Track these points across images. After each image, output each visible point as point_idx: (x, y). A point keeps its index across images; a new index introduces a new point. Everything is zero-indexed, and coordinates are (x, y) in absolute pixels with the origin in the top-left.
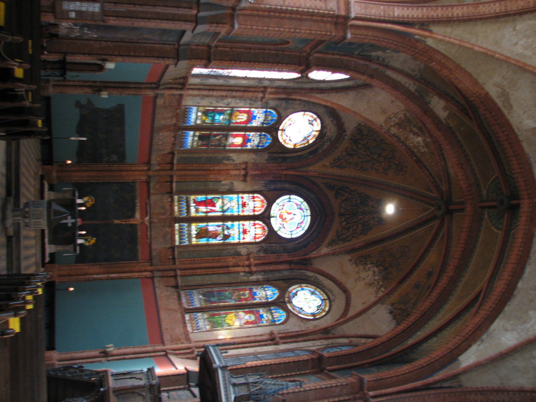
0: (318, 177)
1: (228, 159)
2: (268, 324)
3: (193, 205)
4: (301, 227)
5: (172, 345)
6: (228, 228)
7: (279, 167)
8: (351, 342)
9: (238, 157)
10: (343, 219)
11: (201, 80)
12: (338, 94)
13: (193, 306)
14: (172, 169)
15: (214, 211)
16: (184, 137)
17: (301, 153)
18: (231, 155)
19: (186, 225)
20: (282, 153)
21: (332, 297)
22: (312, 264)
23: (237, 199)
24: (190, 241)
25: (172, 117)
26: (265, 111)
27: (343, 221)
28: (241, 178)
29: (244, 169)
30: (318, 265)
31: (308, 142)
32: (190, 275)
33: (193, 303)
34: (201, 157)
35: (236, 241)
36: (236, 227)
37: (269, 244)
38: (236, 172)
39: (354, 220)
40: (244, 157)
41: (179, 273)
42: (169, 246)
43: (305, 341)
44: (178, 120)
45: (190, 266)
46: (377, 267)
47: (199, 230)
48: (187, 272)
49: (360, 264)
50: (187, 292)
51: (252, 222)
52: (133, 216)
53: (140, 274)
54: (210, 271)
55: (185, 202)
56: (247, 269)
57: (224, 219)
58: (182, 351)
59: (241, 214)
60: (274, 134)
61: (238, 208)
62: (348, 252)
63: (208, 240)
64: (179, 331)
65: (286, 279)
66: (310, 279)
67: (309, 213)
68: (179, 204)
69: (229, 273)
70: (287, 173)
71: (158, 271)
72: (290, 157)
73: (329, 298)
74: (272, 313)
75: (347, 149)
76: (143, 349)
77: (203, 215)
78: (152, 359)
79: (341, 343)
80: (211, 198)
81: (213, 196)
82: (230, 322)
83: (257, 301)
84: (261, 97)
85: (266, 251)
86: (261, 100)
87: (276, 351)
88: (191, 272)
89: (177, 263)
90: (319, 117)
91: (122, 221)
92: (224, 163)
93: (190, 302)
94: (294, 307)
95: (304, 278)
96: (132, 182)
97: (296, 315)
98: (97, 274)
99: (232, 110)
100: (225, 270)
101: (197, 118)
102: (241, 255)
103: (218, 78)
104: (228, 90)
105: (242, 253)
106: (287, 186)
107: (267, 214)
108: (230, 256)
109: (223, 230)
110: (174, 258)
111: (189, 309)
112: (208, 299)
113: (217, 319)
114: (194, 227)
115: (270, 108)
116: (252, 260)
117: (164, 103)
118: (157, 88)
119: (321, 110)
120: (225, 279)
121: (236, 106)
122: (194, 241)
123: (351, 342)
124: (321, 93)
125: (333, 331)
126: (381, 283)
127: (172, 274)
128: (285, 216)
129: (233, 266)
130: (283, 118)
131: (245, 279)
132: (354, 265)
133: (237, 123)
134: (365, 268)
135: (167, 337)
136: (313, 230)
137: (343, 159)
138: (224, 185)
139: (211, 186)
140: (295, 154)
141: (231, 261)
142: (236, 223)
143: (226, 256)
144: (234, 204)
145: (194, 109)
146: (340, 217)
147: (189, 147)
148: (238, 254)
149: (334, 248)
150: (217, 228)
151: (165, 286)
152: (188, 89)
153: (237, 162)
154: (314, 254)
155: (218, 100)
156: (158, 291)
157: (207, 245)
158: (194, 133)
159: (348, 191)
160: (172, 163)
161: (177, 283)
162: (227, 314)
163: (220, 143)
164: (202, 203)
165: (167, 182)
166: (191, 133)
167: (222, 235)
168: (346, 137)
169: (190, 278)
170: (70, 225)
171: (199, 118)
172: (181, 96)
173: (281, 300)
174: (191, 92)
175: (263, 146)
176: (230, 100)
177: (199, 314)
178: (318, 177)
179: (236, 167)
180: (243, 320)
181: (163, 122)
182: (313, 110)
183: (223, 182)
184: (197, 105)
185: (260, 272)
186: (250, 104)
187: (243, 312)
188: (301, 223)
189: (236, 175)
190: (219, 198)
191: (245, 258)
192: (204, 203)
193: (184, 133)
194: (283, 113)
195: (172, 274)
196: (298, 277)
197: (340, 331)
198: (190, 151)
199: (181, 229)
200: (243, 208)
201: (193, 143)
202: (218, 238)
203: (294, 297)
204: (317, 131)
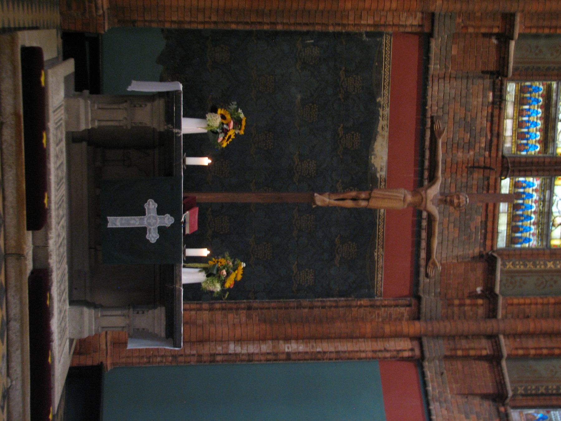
19: (536, 182)
32: (539, 357)
41: (506, 347)
42: (477, 251)
53: (379, 345)
55: (541, 107)
68: (520, 113)
71: (437, 336)
96: (368, 34)
98: (239, 341)
151: (460, 394)
161: (501, 384)
170: (153, 237)
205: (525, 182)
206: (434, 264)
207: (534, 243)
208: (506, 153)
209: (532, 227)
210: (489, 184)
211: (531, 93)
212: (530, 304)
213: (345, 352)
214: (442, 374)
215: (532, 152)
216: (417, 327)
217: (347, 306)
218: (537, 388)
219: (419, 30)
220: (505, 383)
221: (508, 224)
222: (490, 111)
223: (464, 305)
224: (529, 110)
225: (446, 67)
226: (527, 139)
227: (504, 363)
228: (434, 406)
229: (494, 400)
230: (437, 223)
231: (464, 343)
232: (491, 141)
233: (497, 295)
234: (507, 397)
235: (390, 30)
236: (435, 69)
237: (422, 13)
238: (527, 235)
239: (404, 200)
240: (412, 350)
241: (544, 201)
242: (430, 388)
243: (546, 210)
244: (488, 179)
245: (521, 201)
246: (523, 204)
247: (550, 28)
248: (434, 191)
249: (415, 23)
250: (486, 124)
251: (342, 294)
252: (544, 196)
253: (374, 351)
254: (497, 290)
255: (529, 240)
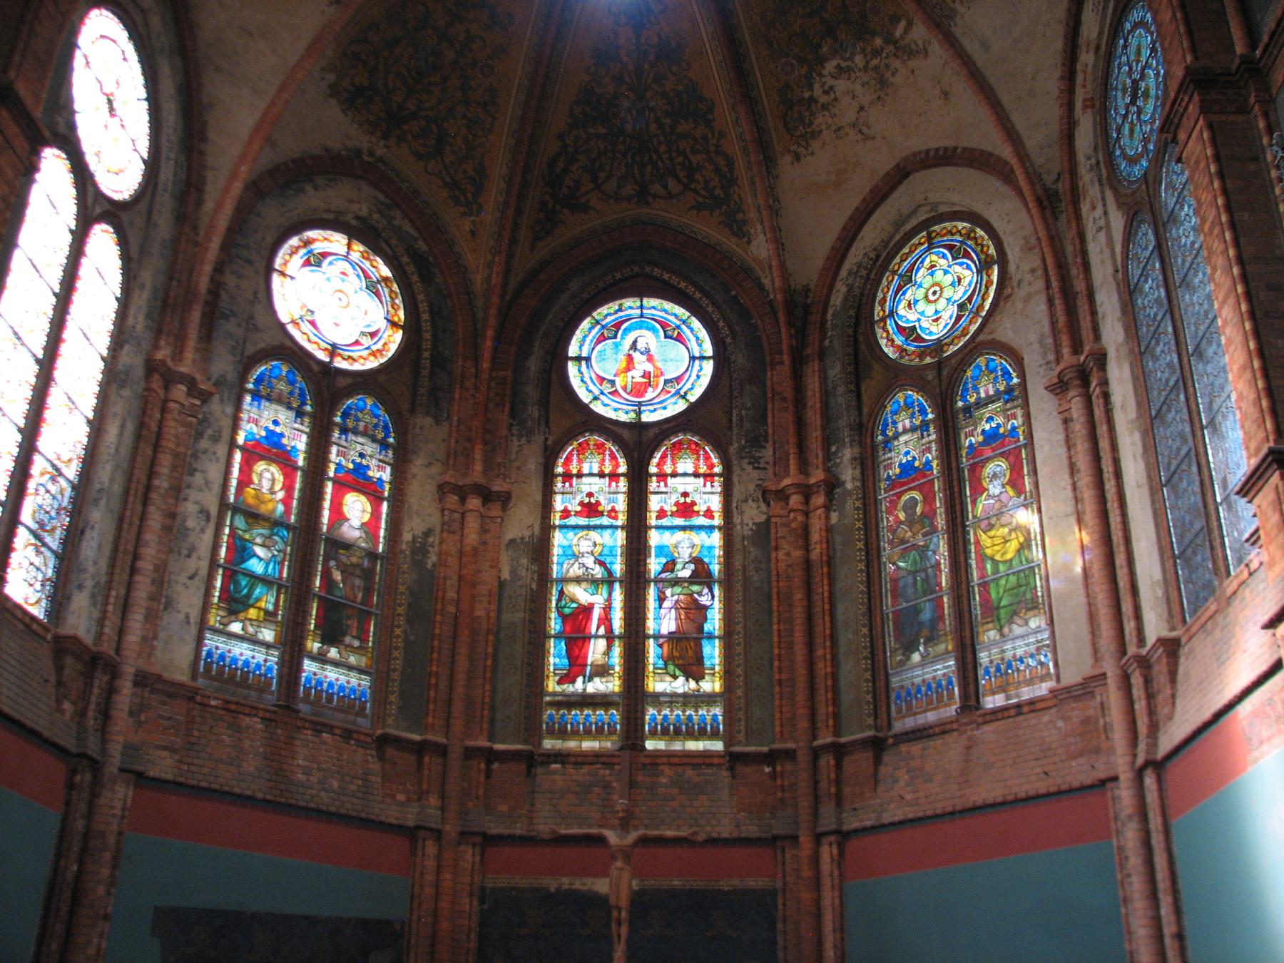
0: (510, 255)
1: (420, 549)
2: (1019, 412)
3: (579, 684)
4: (678, 327)
5: (1112, 750)
6: (670, 566)
7: (468, 384)
8: (1089, 104)
9: (418, 513)
10: (657, 188)
11: (80, 587)
12: (212, 134)
13: (950, 683)
14: (442, 751)
15: (608, 608)
16: (323, 697)
17: (423, 307)
18: (407, 537)
19: (651, 711)
20: (416, 368)
21: (922, 216)
22: (806, 290)
23: (571, 534)
24: (709, 699)
25: (236, 728)
26: (253, 400)
27: (665, 187)
28: (495, 511)
29: (463, 500)
30: (809, 268)
31: (386, 279)
32: (836, 701)
33: (939, 685)
34: (407, 641)
35: (716, 539)
36: (668, 539)
37: (730, 428)
38: (472, 523)
39: (663, 148)
40: (421, 494)
41: (825, 739)
42: (725, 773)
43: (1086, 267)
44: (253, 710)
45: (801, 696)
46: (821, 61)
47: (671, 668)
48: (823, 710)
49: (811, 123)
50: (899, 711)
51: (653, 484)
52: (599, 902)
53: (826, 882)
54: (822, 627)
55: (569, 711)
56: (819, 500)
57: (635, 581)
58: (1140, 706)
59: (622, 519)
60: (342, 382)
61: (602, 527)
62: (770, 164)
63: (711, 636)
64: (1052, 728)
65: (857, 369)
66: (857, 291)
67: (630, 303)
68: (575, 733)
69: (830, 562)
70: (487, 354)
71: (816, 814)
72: (436, 339)
73: (925, 225)
74: (980, 404)
75: (419, 156)
76: (1135, 861)
77: (617, 650)
78: (1177, 825)
79: (1095, 137)
80: (559, 621)
81: (553, 615)
82: (1013, 546)
83: (932, 456)
84: (190, 394)
85: (757, 441)
86: (205, 397)
87: (1131, 352)
88: (823, 696)
89: (790, 745)
90: (297, 228)
91: (616, 939)
92: (434, 565)
93: (936, 693)
94: (952, 335)
95: (852, 312)
96: (482, 902)
97: (986, 320)
99: (236, 509)
100: (819, 573)
101: (253, 641)
102: (768, 521)
103: (81, 525)
104: (145, 502)
105: (763, 518)
106: (533, 365)
107: (626, 434)
108: (769, 560)
109: (676, 582)
110: (771, 758)
111: (965, 696)
112: (925, 632)
113: (1001, 591)
114: (656, 685)
115: (243, 378)
116: (787, 481)
117: (171, 749)
118: (96, 766)
119: (271, 213)
120: (851, 576)
121: (216, 488)
122: (711, 685)
123: (1089, 104)
124: (200, 190)
125: (1049, 179)
126: (878, 42)
127: (827, 761)
128: (636, 375)
129: (807, 548)
130: (288, 343)
131: (851, 504)
132: (815, 145)
133: (286, 502)
134: (825, 107)
135: (1079, 772)
136: (691, 290)
137: (452, 172)
138: (513, 572)
139: (515, 616)
140: (426, 326)
141: (787, 554)
142: (654, 538)
143: (769, 575)
144: (583, 543)
145: (212, 642)
146: (650, 199)
147: (366, 682)
148: (763, 532)
149: (753, 214)
150: (667, 604)
151: (875, 789)
152: (118, 650)
153: (435, 519)
154: (771, 282)
155: (185, 552)
156: (894, 813)
157: (728, 638)
158: (313, 658)
159: (561, 164)
160: (421, 749)
161: (864, 743)
162: (982, 558)
163: (358, 572)
164: (577, 651)
165: (488, 773)
166: (309, 666)
167: (695, 588)
168: (380, 152)
169: (847, 698)
171: (251, 630)
172: (143, 680)
173: (930, 376)
174: (133, 638)
175: (386, 427)
176: (190, 508)
177: (984, 657)
178: (510, 255)
179: (453, 525)
180: (1004, 498)
181: (251, 765)
182: (270, 240)
183: (506, 575)
184: (194, 630)
185: (828, 457)
186: (216, 439)
187: (974, 502)
188: (664, 325)
189: (482, 527)
190: (561, 593)
191: (777, 508)
192: (576, 639)
193: (307, 690)
194: (268, 339)
195: (827, 761)
196: (850, 332)
197: (1046, 157)
198: (379, 672)
199: (664, 732)
200: (601, 514)
201: (350, 668)
202: (704, 600)
203: (919, 339)
204: (349, 246)
205: (649, 724)
206: (694, 834)
207: (718, 711)
208: (617, 747)
209: (700, 713)
210: (650, 764)
211: (554, 723)
212: (781, 712)
213: (834, 922)
214: (855, 809)
215: (618, 718)
216: (805, 839)
217: (785, 921)
218: (868, 703)
219: (478, 848)
220: (862, 739)
221: (697, 739)
222: (571, 766)
223: (782, 786)
224: (572, 724)
225: (520, 817)
226: (603, 724)
227: (843, 740)
228: (887, 819)
229: (883, 750)
230: (649, 832)
231: (823, 785)
232: (603, 763)
233: (770, 750)
234: (875, 737)
235: (476, 879)
236: (521, 829)
237: (459, 844)
238: (709, 718)
239: (621, 869)
240: (831, 844)
241: (671, 702)
242: (869, 823)
243: (681, 699)
244: (644, 765)
245: (672, 727)
246: (674, 725)
247: (483, 709)
248: (612, 837)
249: (470, 851)
250: (585, 769)
251: (772, 925)
252: (666, 702)
253: (833, 887)
254: (765, 749)
255: (715, 715)
